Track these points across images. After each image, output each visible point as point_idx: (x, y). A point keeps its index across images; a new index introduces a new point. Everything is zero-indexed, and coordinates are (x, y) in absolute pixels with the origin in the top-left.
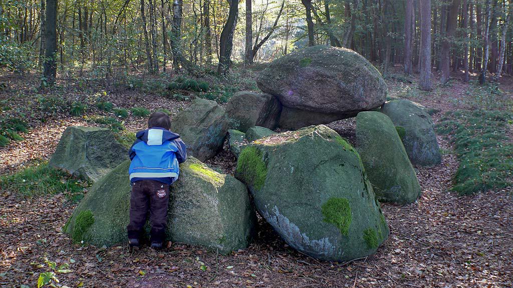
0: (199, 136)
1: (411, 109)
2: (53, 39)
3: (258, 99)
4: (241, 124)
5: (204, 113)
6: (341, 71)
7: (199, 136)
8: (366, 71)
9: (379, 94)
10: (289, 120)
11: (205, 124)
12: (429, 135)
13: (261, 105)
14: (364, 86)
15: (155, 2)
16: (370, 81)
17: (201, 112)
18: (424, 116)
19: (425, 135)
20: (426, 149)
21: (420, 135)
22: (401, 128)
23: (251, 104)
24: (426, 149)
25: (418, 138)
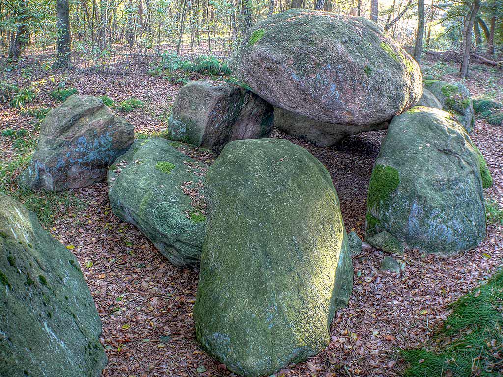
0: (57, 152)
1: (430, 134)
2: (65, 13)
3: (208, 94)
4: (187, 129)
5: (69, 117)
6: (293, 53)
7: (57, 152)
8: (338, 53)
9: (374, 98)
10: (299, 124)
11: (69, 134)
12: (452, 192)
13: (211, 103)
14: (337, 81)
15: (374, 3)
16: (349, 73)
17: (65, 117)
18: (450, 151)
19: (441, 191)
20: (438, 220)
21: (429, 193)
22: (393, 170)
23: (198, 101)
24: (438, 220)
25: (420, 198)
